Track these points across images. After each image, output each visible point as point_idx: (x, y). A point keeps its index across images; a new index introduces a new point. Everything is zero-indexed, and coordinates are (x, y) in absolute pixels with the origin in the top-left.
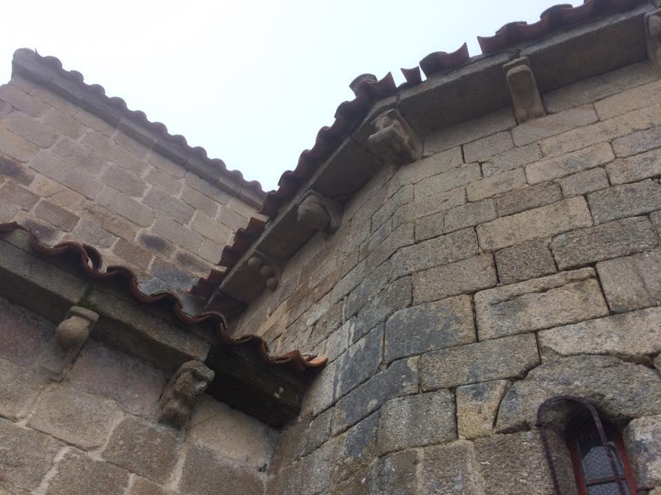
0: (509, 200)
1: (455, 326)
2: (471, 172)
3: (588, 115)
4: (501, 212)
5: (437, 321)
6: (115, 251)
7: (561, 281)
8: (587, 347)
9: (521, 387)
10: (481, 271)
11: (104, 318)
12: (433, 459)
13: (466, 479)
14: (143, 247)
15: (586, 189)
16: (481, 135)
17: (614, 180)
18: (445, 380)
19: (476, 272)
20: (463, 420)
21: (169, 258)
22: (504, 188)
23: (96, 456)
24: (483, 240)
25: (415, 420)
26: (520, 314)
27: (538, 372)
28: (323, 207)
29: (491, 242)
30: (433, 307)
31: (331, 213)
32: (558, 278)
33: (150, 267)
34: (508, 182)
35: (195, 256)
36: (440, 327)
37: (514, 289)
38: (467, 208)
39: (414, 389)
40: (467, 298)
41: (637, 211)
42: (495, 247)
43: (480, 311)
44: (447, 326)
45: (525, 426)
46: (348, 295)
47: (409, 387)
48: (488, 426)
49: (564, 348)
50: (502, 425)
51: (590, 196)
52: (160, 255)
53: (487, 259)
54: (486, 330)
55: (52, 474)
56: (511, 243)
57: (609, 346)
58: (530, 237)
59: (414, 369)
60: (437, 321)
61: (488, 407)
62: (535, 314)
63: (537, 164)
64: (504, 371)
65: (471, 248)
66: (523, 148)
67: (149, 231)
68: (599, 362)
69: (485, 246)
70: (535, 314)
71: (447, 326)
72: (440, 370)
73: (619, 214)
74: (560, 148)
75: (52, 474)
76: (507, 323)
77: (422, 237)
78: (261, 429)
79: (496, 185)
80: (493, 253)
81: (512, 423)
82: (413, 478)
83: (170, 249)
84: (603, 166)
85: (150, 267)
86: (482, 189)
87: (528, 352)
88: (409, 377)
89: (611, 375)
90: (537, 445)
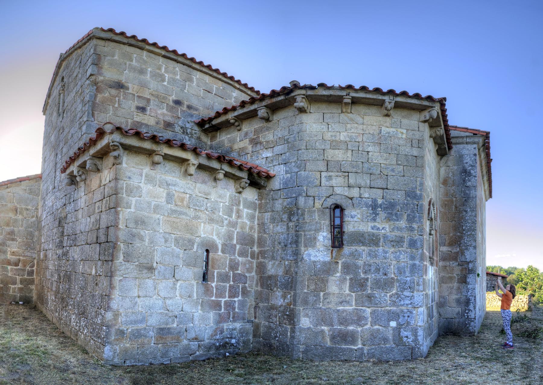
0: (334, 144)
1: (316, 181)
2: (325, 127)
3: (360, 120)
4: (332, 148)
5: (311, 178)
6: (167, 110)
7: (341, 175)
8: (342, 193)
9: (328, 199)
10: (277, 379)
11: (226, 172)
12: (309, 211)
13: (315, 216)
14: (174, 105)
15: (353, 149)
16: (330, 111)
17: (359, 149)
18: (312, 194)
19: (322, 166)
20: (316, 204)
21: (184, 108)
22: (333, 138)
23: (227, 204)
24: (325, 155)
25: (305, 203)
26: (331, 181)
27: (331, 197)
28: (267, 113)
29: (327, 157)
30: (311, 173)
31: (270, 115)
32: (340, 174)
33: (179, 114)
34: (335, 136)
35: (192, 105)
36: (312, 180)
37: (331, 174)
38: (322, 141)
39: (305, 195)
40: (319, 173)
41: (361, 161)
42: (328, 159)
43: (322, 178)
44: (314, 180)
45: (328, 208)
46: (281, 154)
47: (304, 194)
48: (320, 206)
49: (338, 192)
50: (323, 207)
51: (353, 151)
52: (181, 107)
53: (326, 162)
54: (323, 184)
55: (221, 210)
56: (332, 159)
57: (346, 194)
58: (337, 159)
59: (305, 190)
60: (311, 178)
61: (321, 202)
62: (334, 182)
63: (344, 133)
64: (325, 195)
65: (322, 157)
66: (342, 124)
67: (174, 97)
68: (343, 197)
69: (326, 158)
70: (334, 182)
71: (314, 180)
72: (311, 192)
73: (357, 160)
74: (351, 130)
75: (221, 210)
76: (328, 183)
77: (309, 148)
78: (177, 164)
79: (332, 136)
80: (327, 161)
81: (325, 207)
82: (304, 215)
83: (183, 104)
84: (359, 142)
85: (179, 114)
86: (328, 136)
87: (330, 192)
88: (304, 192)
89: (344, 201)
90: (329, 212)
